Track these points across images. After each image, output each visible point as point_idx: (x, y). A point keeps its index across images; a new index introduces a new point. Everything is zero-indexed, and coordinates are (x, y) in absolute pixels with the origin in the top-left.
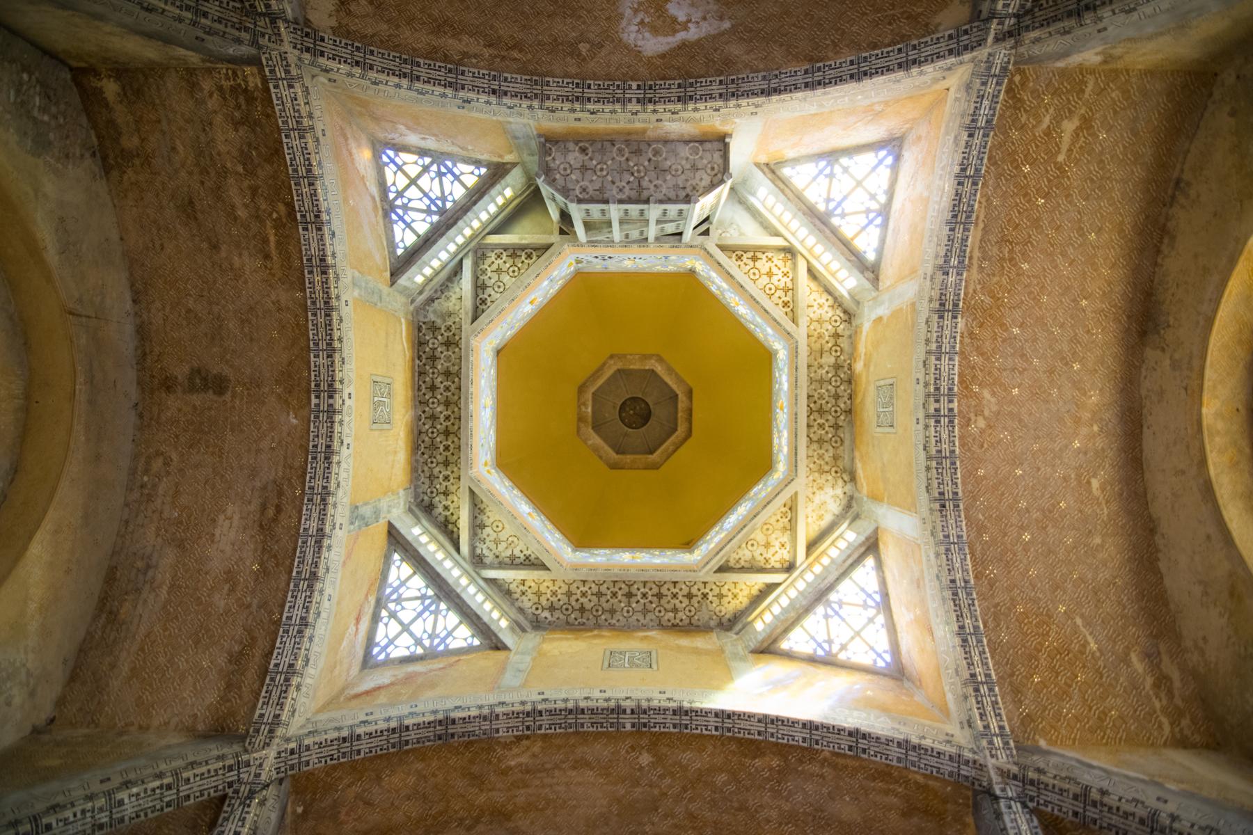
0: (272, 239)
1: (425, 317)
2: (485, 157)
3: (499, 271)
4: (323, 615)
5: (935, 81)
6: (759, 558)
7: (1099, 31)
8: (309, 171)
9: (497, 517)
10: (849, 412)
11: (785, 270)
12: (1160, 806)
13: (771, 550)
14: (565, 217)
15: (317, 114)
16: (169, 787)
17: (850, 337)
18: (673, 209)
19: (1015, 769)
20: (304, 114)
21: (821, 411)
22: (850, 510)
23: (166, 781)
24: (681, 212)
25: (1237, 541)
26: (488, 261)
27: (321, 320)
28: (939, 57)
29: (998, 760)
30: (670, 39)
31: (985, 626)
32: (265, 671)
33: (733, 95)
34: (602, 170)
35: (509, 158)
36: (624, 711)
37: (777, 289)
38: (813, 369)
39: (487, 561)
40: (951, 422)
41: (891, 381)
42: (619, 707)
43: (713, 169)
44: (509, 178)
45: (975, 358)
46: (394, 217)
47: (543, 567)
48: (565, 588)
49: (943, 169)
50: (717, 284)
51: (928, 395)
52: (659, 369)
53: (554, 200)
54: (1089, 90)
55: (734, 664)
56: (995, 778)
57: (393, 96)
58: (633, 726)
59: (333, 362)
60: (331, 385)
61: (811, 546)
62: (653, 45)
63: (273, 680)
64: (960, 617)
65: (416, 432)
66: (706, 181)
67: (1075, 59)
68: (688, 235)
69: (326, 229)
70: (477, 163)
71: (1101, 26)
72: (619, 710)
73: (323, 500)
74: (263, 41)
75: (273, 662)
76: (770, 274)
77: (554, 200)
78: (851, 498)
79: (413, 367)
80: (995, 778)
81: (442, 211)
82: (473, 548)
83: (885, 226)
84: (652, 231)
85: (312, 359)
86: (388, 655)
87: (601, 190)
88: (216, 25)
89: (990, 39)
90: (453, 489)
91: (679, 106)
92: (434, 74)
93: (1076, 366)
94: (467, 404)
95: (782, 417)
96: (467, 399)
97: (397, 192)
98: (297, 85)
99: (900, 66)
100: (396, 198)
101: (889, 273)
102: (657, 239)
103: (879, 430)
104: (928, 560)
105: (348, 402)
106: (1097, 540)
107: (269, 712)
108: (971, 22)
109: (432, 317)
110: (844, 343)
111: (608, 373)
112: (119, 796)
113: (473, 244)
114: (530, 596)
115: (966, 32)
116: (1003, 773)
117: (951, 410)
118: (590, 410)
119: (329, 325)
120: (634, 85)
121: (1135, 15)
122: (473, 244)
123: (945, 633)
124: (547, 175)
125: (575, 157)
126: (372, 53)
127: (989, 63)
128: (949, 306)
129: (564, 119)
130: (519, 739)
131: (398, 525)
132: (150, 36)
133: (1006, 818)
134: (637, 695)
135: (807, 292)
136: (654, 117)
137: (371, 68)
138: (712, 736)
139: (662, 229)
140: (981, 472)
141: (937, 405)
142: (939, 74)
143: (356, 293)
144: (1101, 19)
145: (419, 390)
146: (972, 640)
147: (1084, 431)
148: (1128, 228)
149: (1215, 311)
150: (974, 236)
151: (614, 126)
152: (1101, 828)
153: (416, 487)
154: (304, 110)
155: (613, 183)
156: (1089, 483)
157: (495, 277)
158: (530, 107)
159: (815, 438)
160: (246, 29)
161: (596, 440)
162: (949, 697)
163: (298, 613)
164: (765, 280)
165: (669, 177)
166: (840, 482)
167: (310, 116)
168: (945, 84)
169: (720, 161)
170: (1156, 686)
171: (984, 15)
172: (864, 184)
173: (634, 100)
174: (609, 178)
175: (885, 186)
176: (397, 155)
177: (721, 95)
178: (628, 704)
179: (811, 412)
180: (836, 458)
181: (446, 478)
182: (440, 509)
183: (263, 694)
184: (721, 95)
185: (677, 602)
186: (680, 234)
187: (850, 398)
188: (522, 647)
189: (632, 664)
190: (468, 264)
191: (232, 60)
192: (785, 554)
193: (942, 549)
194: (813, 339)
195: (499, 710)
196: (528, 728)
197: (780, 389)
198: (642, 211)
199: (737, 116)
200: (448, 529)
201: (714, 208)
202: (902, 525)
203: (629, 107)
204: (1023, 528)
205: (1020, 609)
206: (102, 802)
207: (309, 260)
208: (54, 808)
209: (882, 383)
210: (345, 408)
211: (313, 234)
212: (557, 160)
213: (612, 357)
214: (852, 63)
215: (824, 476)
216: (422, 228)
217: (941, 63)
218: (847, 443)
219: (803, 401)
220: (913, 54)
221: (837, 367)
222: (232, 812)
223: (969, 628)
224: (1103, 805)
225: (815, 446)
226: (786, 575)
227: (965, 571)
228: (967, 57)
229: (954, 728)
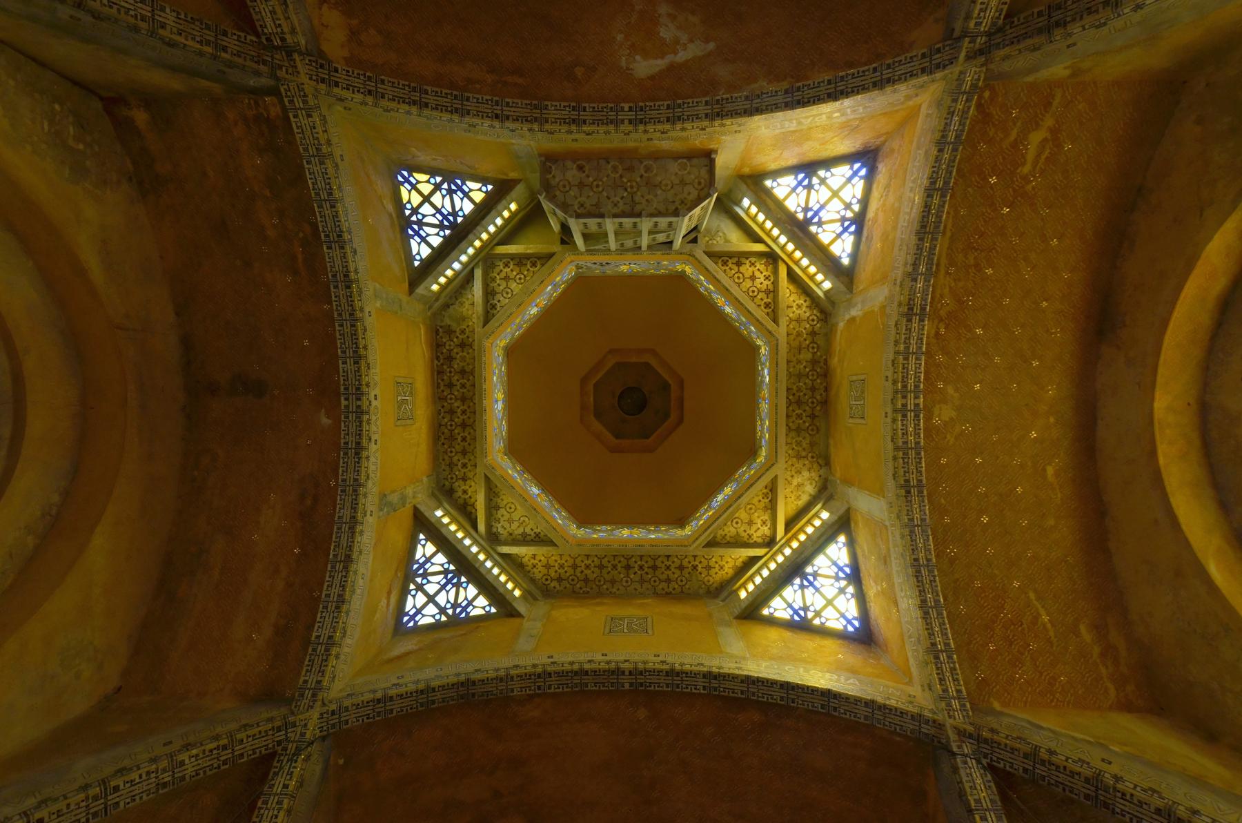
0: (300, 257)
3: (507, 278)
4: (358, 591)
5: (908, 98)
6: (743, 534)
7: (1068, 47)
8: (330, 194)
9: (510, 500)
10: (825, 403)
11: (767, 274)
12: (1105, 766)
13: (754, 527)
14: (565, 229)
15: (334, 140)
16: (225, 747)
17: (826, 335)
18: (663, 222)
19: (970, 729)
20: (323, 142)
21: (799, 403)
22: (824, 493)
23: (222, 742)
24: (670, 224)
25: (1184, 527)
26: (497, 270)
27: (347, 330)
28: (912, 75)
30: (659, 62)
31: (945, 600)
32: (307, 642)
33: (718, 115)
34: (598, 186)
35: (513, 175)
36: (623, 673)
37: (759, 291)
39: (502, 538)
40: (917, 416)
41: (863, 377)
42: (618, 669)
43: (700, 183)
44: (514, 194)
45: (940, 357)
46: (410, 232)
47: (551, 543)
48: (571, 562)
49: (914, 181)
50: (705, 285)
51: (896, 392)
52: (653, 362)
53: (555, 214)
54: (1056, 103)
55: (721, 629)
56: (953, 736)
57: (406, 121)
58: (631, 685)
59: (359, 368)
60: (358, 389)
62: (644, 67)
63: (314, 650)
64: (922, 592)
66: (694, 194)
67: (1044, 74)
68: (678, 243)
69: (348, 249)
71: (1070, 41)
72: (618, 672)
73: (355, 491)
74: (281, 73)
75: (314, 634)
76: (753, 278)
77: (555, 214)
78: (826, 480)
79: (432, 367)
80: (953, 736)
81: (458, 573)
82: (489, 526)
83: (858, 233)
84: (645, 241)
85: (341, 366)
86: (416, 622)
87: (597, 205)
88: (236, 59)
90: (470, 475)
91: (668, 126)
92: (442, 101)
93: (1035, 363)
94: (481, 400)
96: (481, 395)
97: (412, 209)
98: (315, 114)
99: (875, 85)
100: (411, 215)
101: (864, 275)
102: (650, 247)
103: (851, 420)
104: (895, 540)
105: (374, 403)
106: (1051, 522)
107: (312, 679)
108: (944, 40)
109: (448, 321)
110: (820, 340)
111: (609, 364)
112: (180, 757)
113: (483, 254)
114: (540, 568)
115: (938, 51)
116: (961, 733)
117: (917, 405)
120: (626, 106)
121: (1105, 29)
122: (483, 254)
123: (908, 603)
124: (547, 192)
125: (572, 174)
126: (383, 82)
127: (960, 79)
128: (917, 310)
129: (564, 140)
130: (531, 697)
131: (422, 508)
132: (173, 69)
133: (962, 772)
134: (636, 658)
135: (787, 291)
136: (645, 137)
137: (383, 97)
138: (700, 694)
139: (654, 239)
140: (944, 461)
141: (904, 401)
142: (911, 92)
143: (378, 305)
144: (1070, 35)
145: (438, 387)
146: (933, 613)
149: (1171, 313)
150: (942, 245)
151: (608, 145)
152: (1049, 784)
154: (323, 138)
155: (608, 198)
156: (1044, 470)
157: (504, 284)
158: (530, 130)
159: (793, 427)
160: (265, 63)
161: (597, 426)
162: (912, 661)
163: (335, 591)
164: (748, 283)
165: (659, 192)
166: (815, 465)
167: (329, 143)
168: (918, 100)
169: (706, 176)
170: (1103, 655)
171: (957, 34)
172: (841, 194)
173: (626, 122)
174: (605, 194)
176: (411, 175)
177: (707, 115)
178: (626, 666)
179: (789, 403)
180: (812, 444)
181: (464, 466)
182: (460, 493)
183: (306, 663)
184: (707, 115)
185: (670, 573)
186: (671, 243)
187: (826, 389)
188: (535, 617)
189: (630, 630)
190: (478, 273)
191: (254, 91)
192: (766, 530)
193: (907, 532)
194: (792, 337)
195: (512, 672)
196: (539, 688)
197: (763, 381)
198: (635, 224)
199: (725, 134)
200: (466, 513)
201: (701, 219)
202: (871, 506)
203: (622, 128)
204: (982, 512)
205: (978, 584)
206: (164, 764)
207: (334, 276)
208: (121, 771)
209: (854, 378)
210: (372, 408)
211: (337, 253)
212: (557, 176)
213: (611, 351)
214: (829, 82)
215: (802, 461)
216: (472, 591)
217: (914, 81)
220: (887, 73)
221: (814, 362)
222: (281, 768)
223: (931, 603)
224: (1051, 763)
225: (793, 434)
226: (766, 550)
227: (944, 634)
228: (938, 75)
229: (916, 690)
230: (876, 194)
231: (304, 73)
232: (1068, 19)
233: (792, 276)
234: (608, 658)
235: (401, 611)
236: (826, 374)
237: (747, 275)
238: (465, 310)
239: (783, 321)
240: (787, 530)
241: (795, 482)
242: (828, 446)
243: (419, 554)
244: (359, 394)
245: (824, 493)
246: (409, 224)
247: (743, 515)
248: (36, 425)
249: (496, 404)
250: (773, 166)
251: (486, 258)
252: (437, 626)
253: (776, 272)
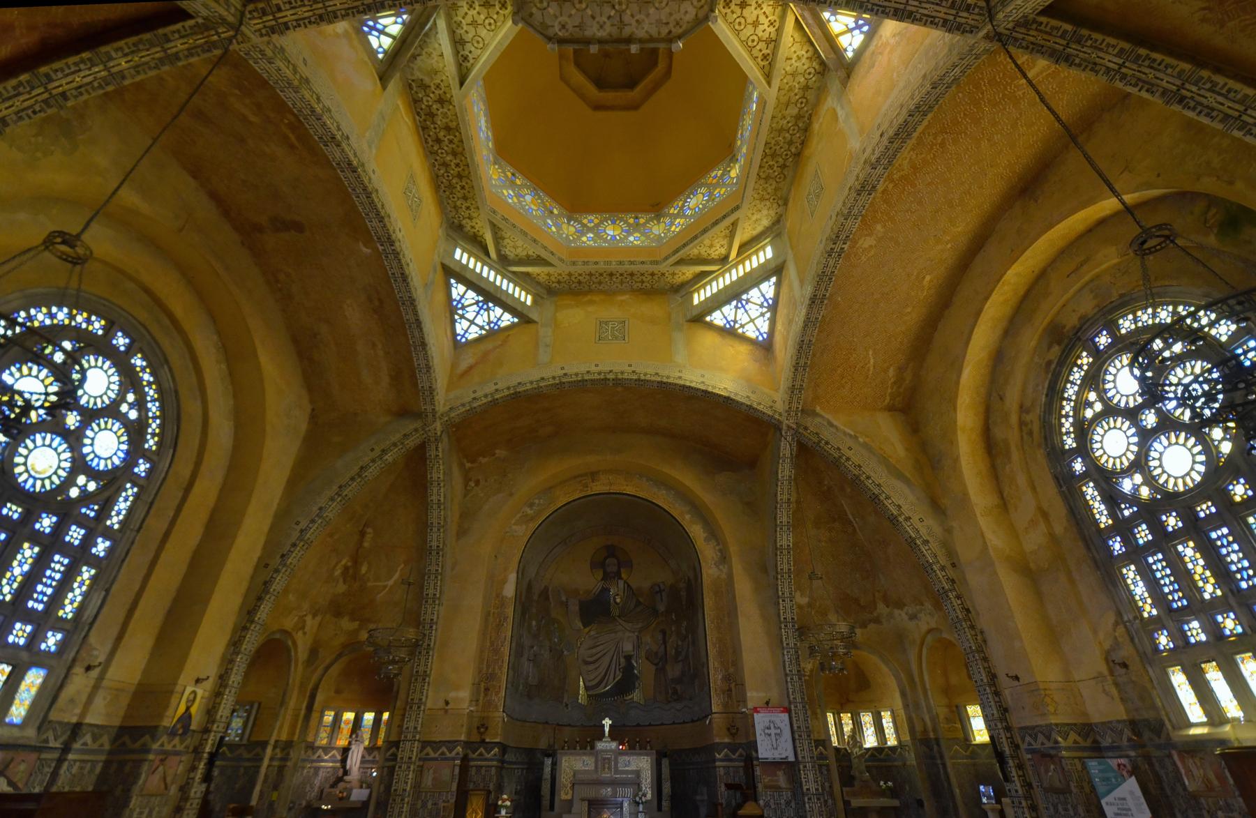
1: (412, 74)
3: (474, 23)
10: (798, 155)
21: (774, 155)
22: (774, 231)
26: (461, 12)
29: (786, 422)
37: (760, 40)
46: (366, 29)
56: (785, 427)
61: (744, 247)
70: (448, 287)
76: (756, 24)
81: (485, 302)
87: (581, 26)
89: (981, 34)
90: (475, 215)
94: (472, 159)
109: (418, 75)
134: (617, 369)
145: (427, 142)
147: (939, 247)
155: (593, 18)
157: (472, 30)
159: (763, 175)
164: (749, 31)
165: (652, 11)
166: (775, 205)
174: (589, 12)
180: (776, 190)
187: (802, 143)
192: (723, 251)
194: (783, 92)
200: (477, 245)
216: (498, 311)
219: (761, 147)
221: (799, 117)
225: (762, 182)
232: (1077, 61)
234: (598, 369)
235: (455, 334)
236: (806, 130)
237: (750, 20)
238: (434, 62)
240: (739, 254)
241: (754, 218)
243: (455, 295)
245: (774, 231)
247: (707, 242)
248: (179, 312)
252: (480, 339)
253: (783, 17)
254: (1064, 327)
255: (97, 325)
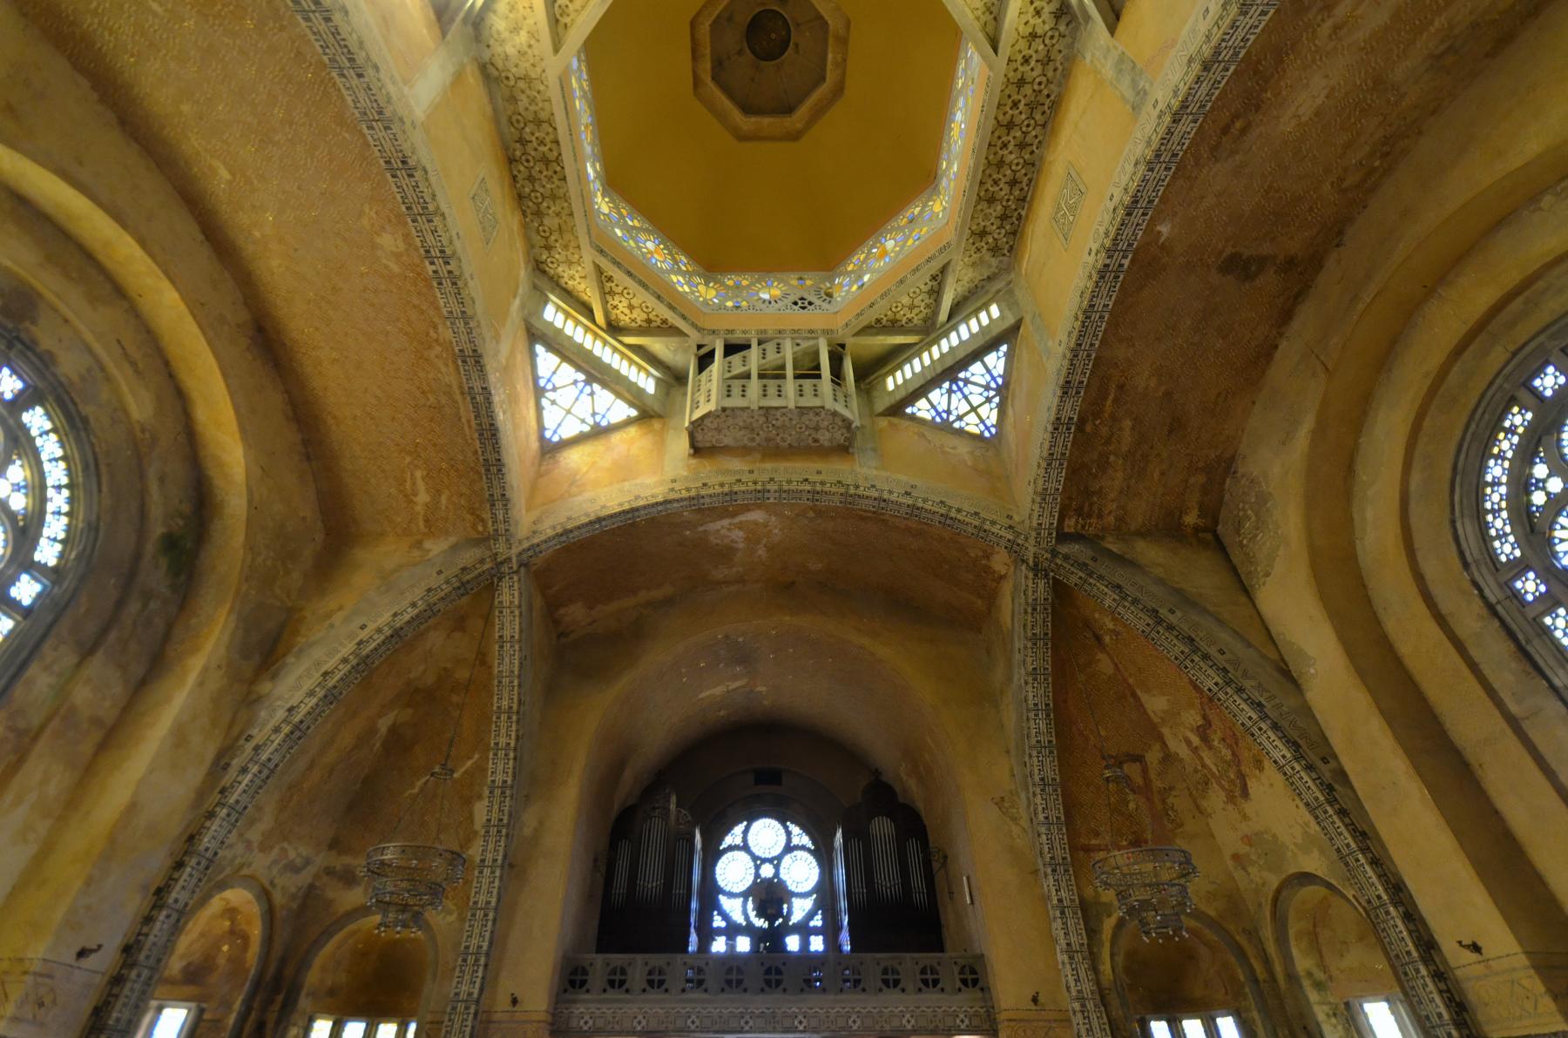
2: (905, 423)
10: (511, 161)
17: (533, 247)
21: (546, 161)
35: (883, 422)
38: (566, 211)
52: (737, 116)
61: (639, 350)
65: (1049, 126)
70: (913, 417)
76: (631, 307)
79: (1029, 209)
90: (1022, 44)
94: (976, 165)
95: (587, 141)
106: (185, 108)
109: (994, 262)
111: (802, 112)
118: (830, 56)
119: (1081, 335)
122: (933, 336)
135: (591, 295)
142: (540, 527)
144: (447, 582)
145: (1030, 180)
148: (330, 421)
153: (1071, 46)
156: (233, 175)
157: (916, 302)
158: (857, 487)
175: (545, 413)
179: (558, 160)
180: (513, 99)
181: (1026, 60)
187: (514, 177)
190: (943, 316)
194: (573, 244)
199: (686, 478)
215: (520, 72)
216: (977, 368)
218: (504, 120)
221: (539, 214)
225: (543, 115)
230: (533, 423)
231: (1031, 551)
233: (588, 311)
239: (590, 268)
242: (492, 98)
244: (1103, 273)
246: (999, 390)
249: (963, 126)
250: (727, 889)
251: (930, 331)
254: (34, 322)
255: (1518, 420)
